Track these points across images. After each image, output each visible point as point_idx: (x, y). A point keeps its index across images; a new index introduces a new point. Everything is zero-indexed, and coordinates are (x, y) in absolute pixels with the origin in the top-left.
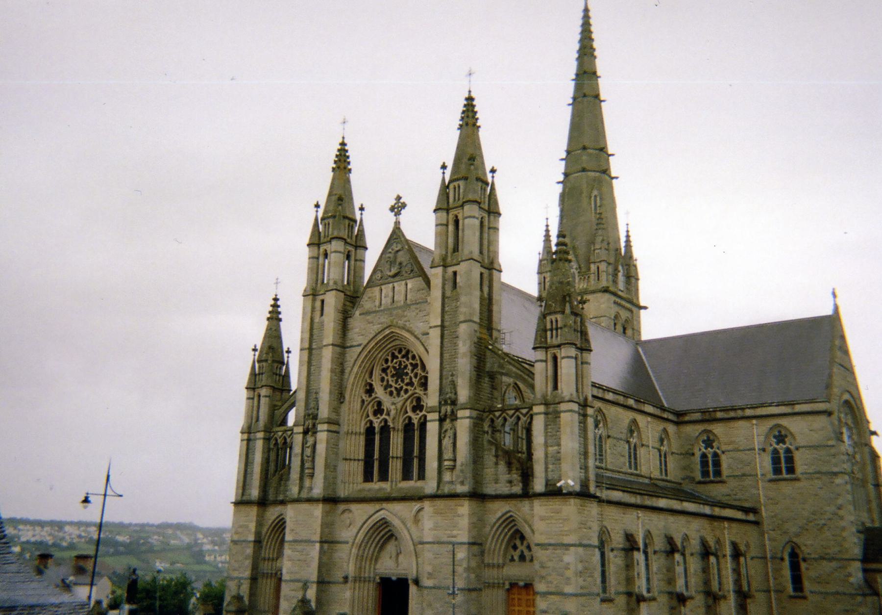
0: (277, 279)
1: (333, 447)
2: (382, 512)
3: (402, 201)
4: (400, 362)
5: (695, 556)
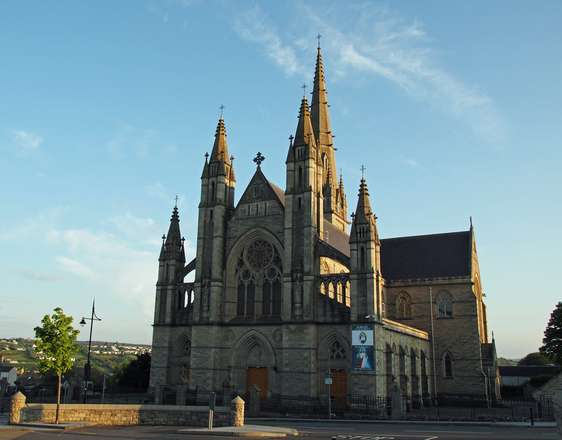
0: (177, 196)
1: (222, 295)
2: (252, 332)
3: (261, 156)
4: (260, 248)
5: (397, 355)
